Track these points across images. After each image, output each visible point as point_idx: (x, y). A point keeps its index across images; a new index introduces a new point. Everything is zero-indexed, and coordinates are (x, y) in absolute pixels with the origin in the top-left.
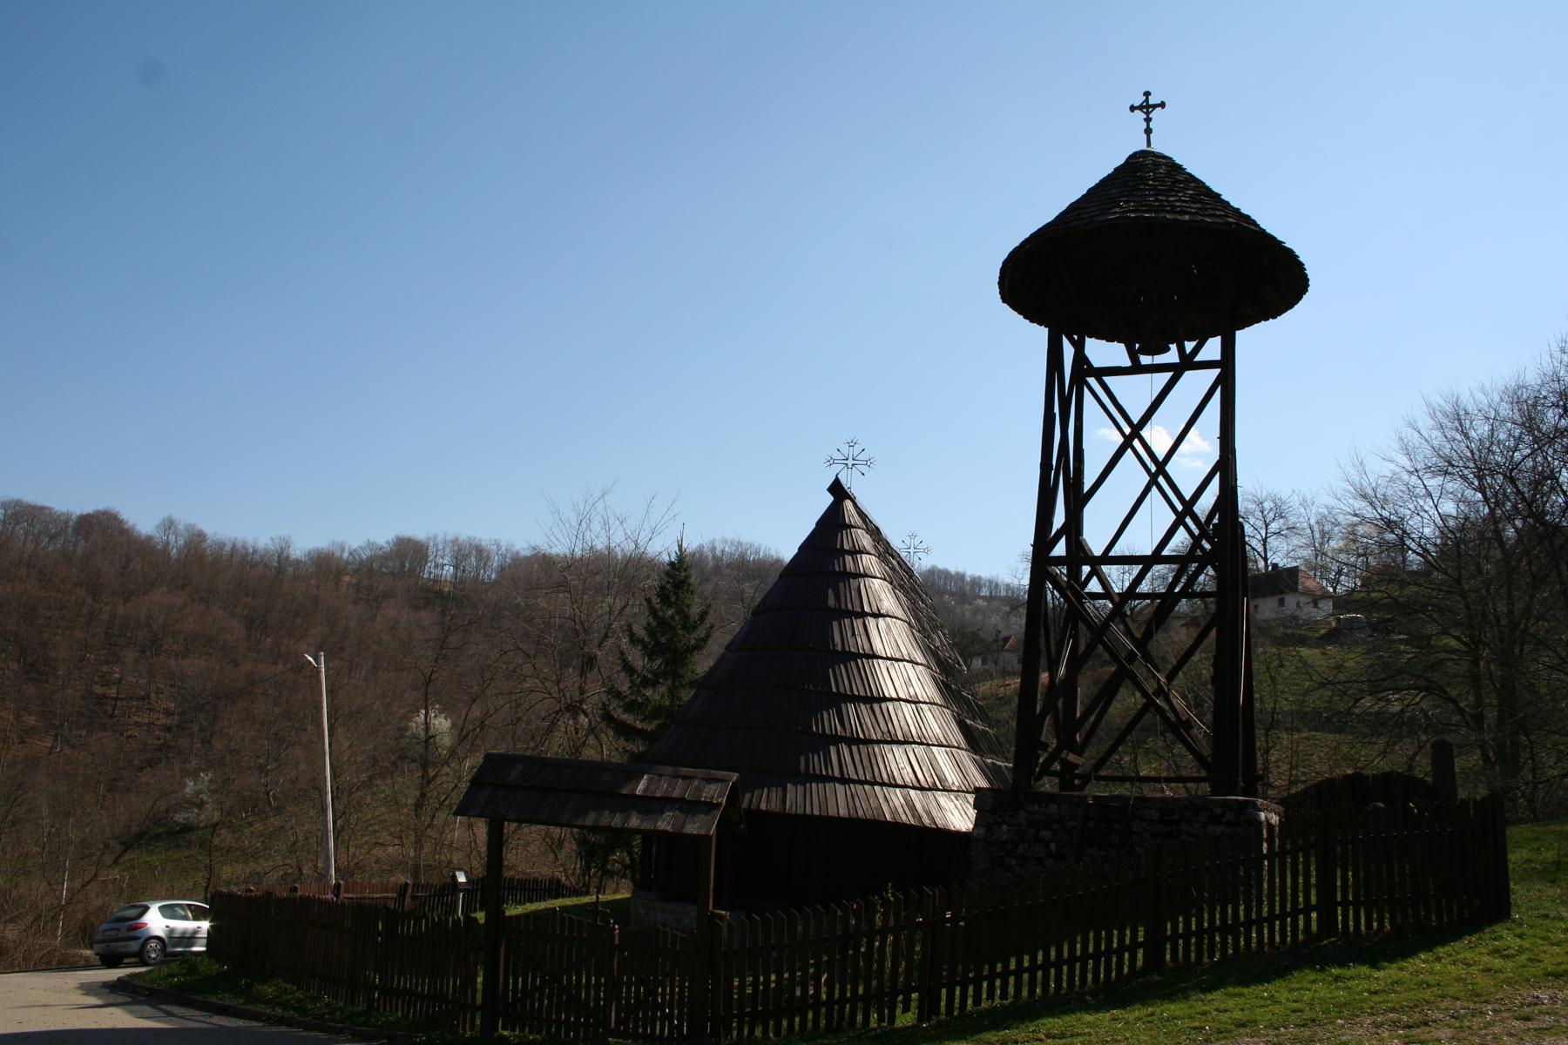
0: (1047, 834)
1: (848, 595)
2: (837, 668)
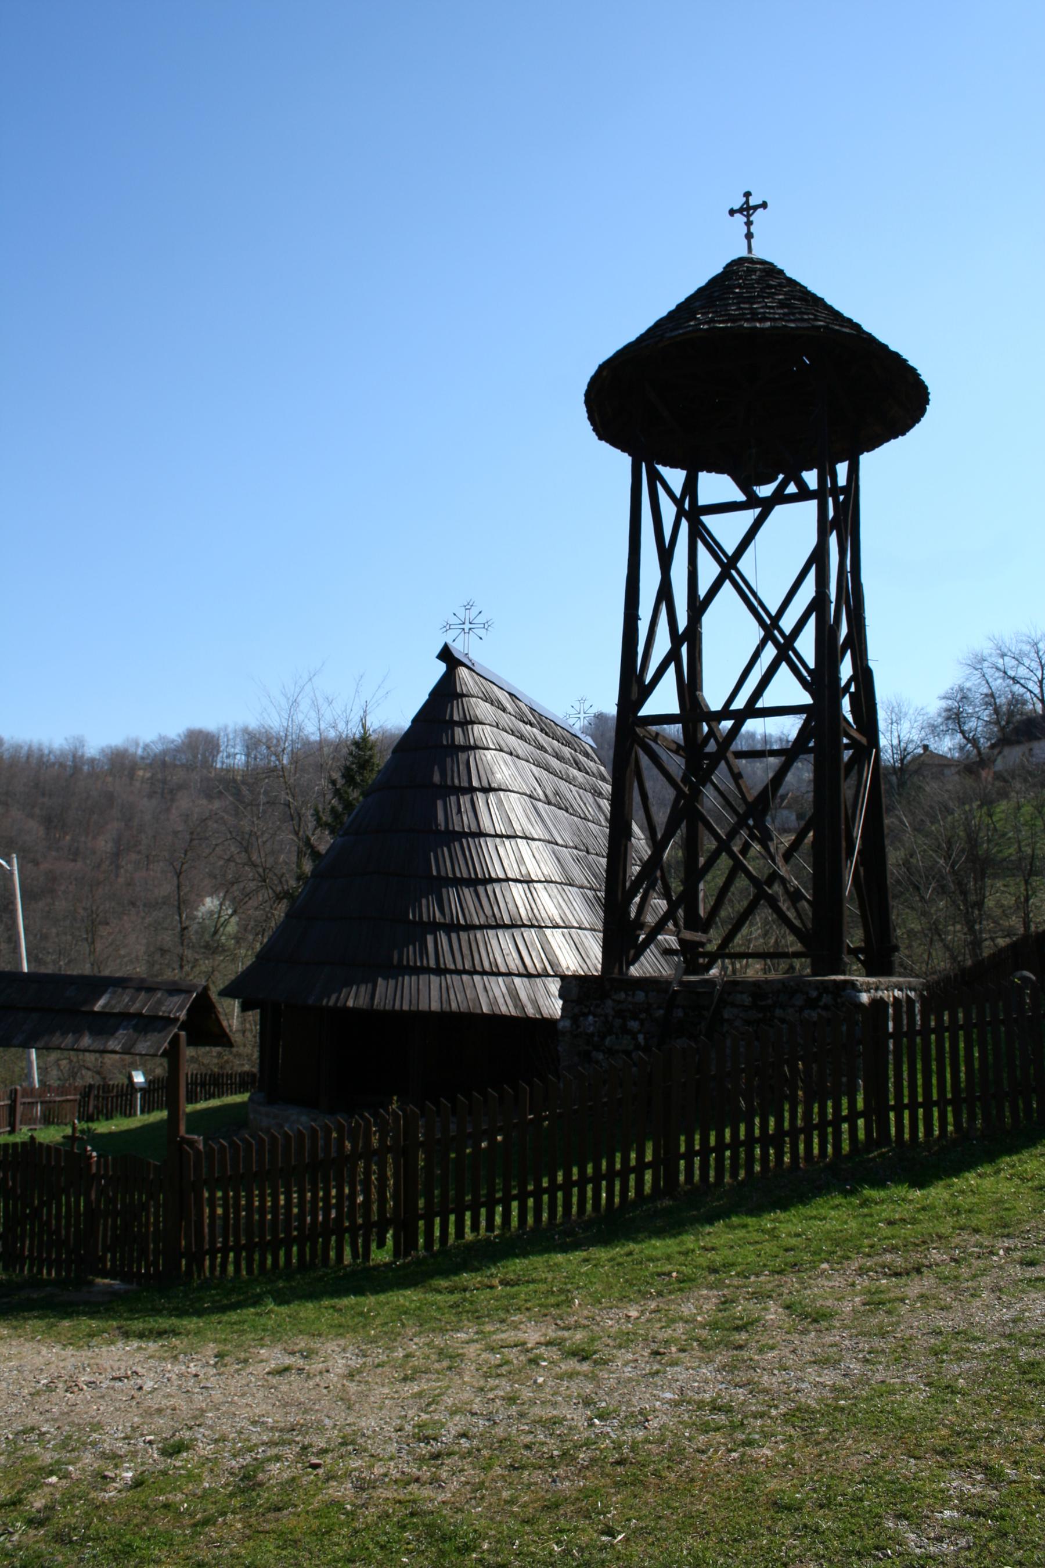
0: (634, 1025)
1: (456, 769)
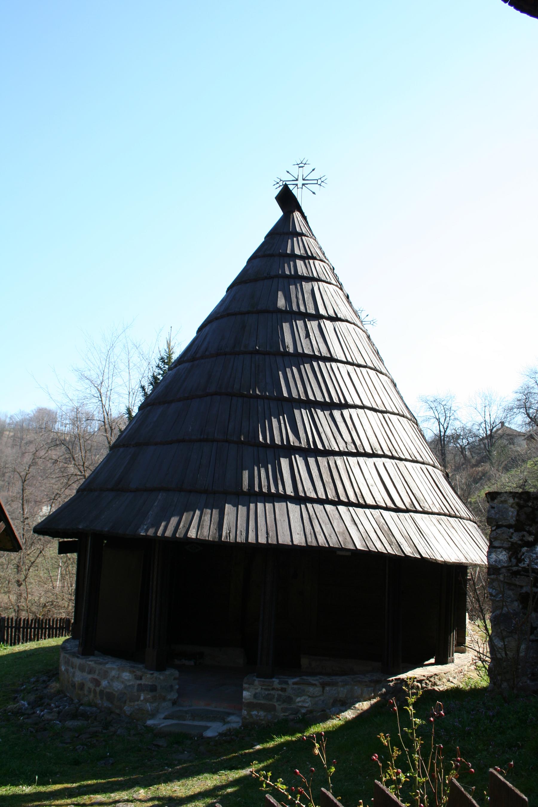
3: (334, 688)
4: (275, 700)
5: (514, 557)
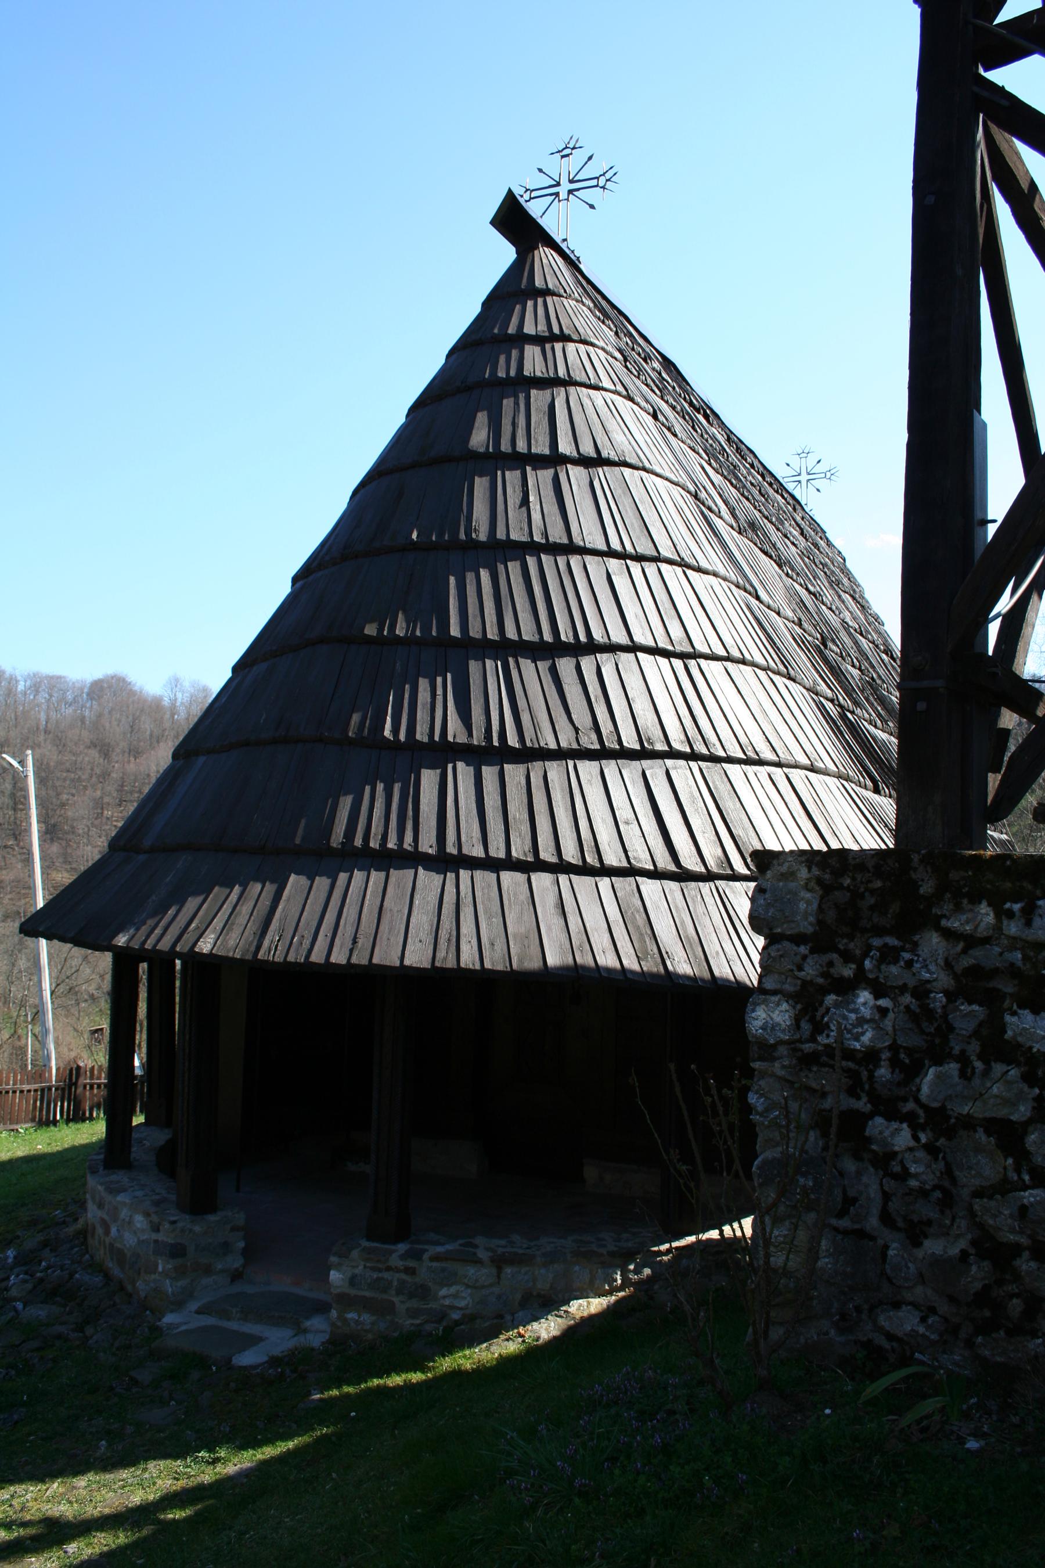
2: (470, 577)
3: (523, 1270)
4: (394, 1292)
5: (807, 1018)
